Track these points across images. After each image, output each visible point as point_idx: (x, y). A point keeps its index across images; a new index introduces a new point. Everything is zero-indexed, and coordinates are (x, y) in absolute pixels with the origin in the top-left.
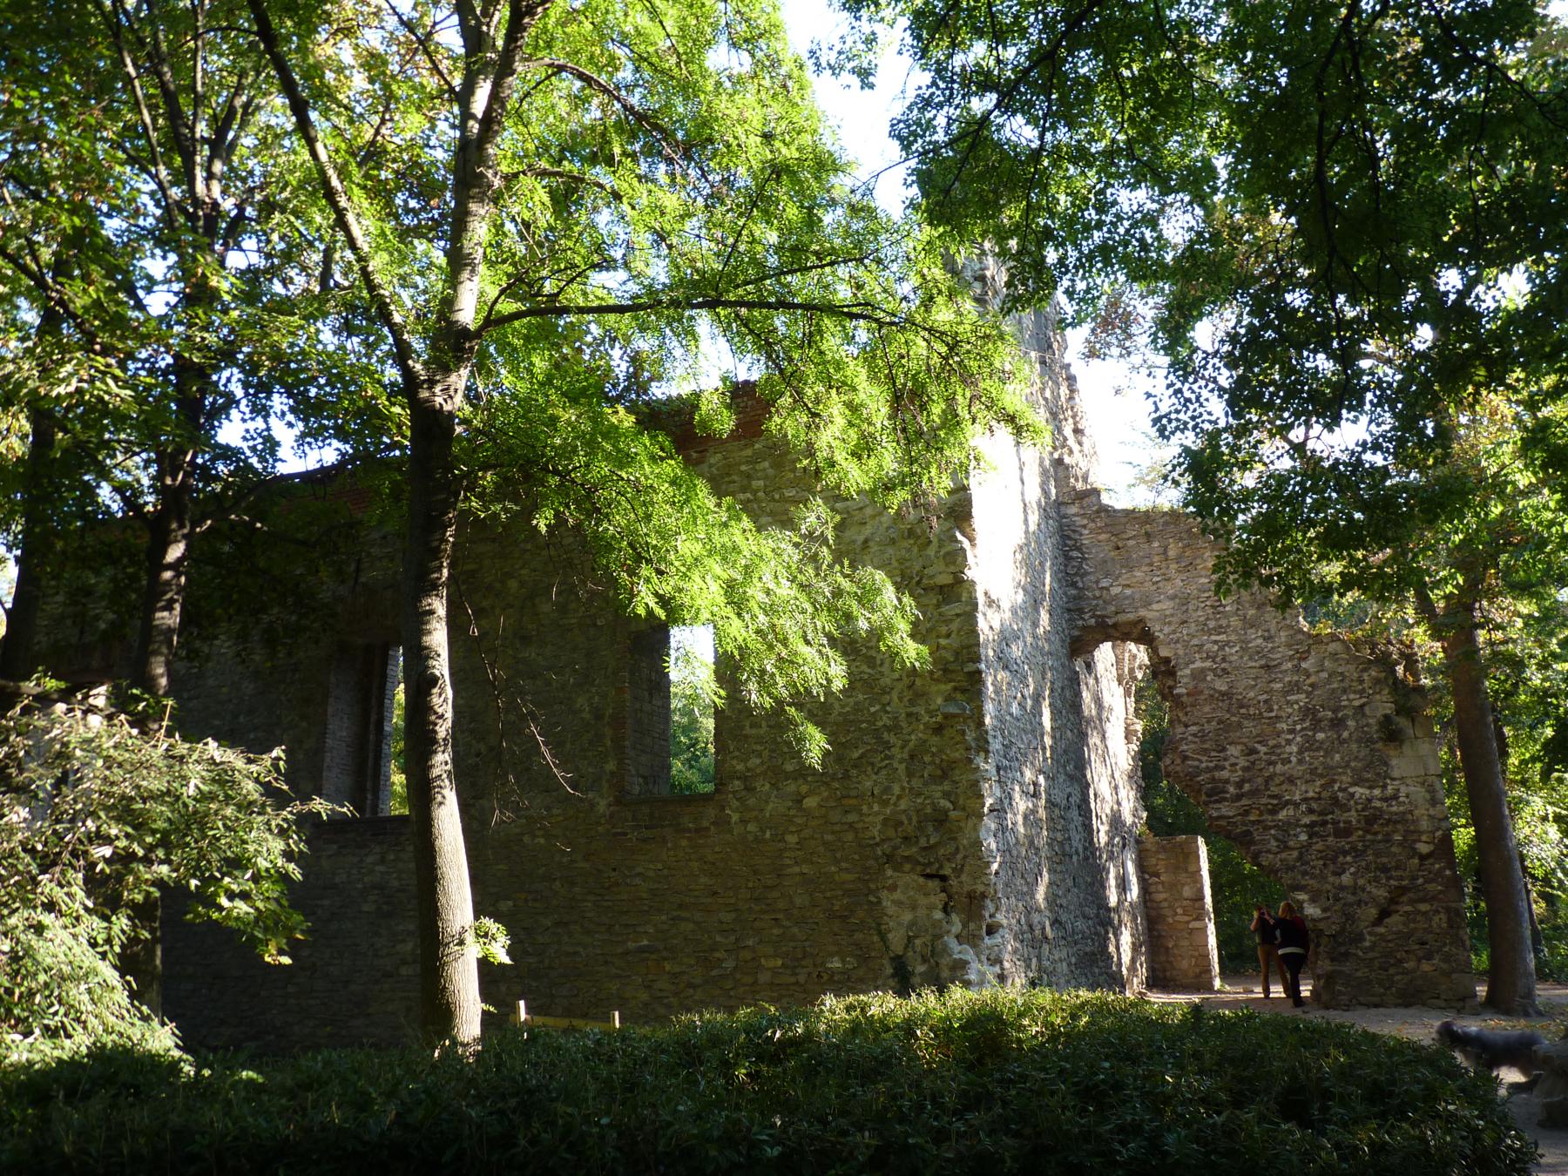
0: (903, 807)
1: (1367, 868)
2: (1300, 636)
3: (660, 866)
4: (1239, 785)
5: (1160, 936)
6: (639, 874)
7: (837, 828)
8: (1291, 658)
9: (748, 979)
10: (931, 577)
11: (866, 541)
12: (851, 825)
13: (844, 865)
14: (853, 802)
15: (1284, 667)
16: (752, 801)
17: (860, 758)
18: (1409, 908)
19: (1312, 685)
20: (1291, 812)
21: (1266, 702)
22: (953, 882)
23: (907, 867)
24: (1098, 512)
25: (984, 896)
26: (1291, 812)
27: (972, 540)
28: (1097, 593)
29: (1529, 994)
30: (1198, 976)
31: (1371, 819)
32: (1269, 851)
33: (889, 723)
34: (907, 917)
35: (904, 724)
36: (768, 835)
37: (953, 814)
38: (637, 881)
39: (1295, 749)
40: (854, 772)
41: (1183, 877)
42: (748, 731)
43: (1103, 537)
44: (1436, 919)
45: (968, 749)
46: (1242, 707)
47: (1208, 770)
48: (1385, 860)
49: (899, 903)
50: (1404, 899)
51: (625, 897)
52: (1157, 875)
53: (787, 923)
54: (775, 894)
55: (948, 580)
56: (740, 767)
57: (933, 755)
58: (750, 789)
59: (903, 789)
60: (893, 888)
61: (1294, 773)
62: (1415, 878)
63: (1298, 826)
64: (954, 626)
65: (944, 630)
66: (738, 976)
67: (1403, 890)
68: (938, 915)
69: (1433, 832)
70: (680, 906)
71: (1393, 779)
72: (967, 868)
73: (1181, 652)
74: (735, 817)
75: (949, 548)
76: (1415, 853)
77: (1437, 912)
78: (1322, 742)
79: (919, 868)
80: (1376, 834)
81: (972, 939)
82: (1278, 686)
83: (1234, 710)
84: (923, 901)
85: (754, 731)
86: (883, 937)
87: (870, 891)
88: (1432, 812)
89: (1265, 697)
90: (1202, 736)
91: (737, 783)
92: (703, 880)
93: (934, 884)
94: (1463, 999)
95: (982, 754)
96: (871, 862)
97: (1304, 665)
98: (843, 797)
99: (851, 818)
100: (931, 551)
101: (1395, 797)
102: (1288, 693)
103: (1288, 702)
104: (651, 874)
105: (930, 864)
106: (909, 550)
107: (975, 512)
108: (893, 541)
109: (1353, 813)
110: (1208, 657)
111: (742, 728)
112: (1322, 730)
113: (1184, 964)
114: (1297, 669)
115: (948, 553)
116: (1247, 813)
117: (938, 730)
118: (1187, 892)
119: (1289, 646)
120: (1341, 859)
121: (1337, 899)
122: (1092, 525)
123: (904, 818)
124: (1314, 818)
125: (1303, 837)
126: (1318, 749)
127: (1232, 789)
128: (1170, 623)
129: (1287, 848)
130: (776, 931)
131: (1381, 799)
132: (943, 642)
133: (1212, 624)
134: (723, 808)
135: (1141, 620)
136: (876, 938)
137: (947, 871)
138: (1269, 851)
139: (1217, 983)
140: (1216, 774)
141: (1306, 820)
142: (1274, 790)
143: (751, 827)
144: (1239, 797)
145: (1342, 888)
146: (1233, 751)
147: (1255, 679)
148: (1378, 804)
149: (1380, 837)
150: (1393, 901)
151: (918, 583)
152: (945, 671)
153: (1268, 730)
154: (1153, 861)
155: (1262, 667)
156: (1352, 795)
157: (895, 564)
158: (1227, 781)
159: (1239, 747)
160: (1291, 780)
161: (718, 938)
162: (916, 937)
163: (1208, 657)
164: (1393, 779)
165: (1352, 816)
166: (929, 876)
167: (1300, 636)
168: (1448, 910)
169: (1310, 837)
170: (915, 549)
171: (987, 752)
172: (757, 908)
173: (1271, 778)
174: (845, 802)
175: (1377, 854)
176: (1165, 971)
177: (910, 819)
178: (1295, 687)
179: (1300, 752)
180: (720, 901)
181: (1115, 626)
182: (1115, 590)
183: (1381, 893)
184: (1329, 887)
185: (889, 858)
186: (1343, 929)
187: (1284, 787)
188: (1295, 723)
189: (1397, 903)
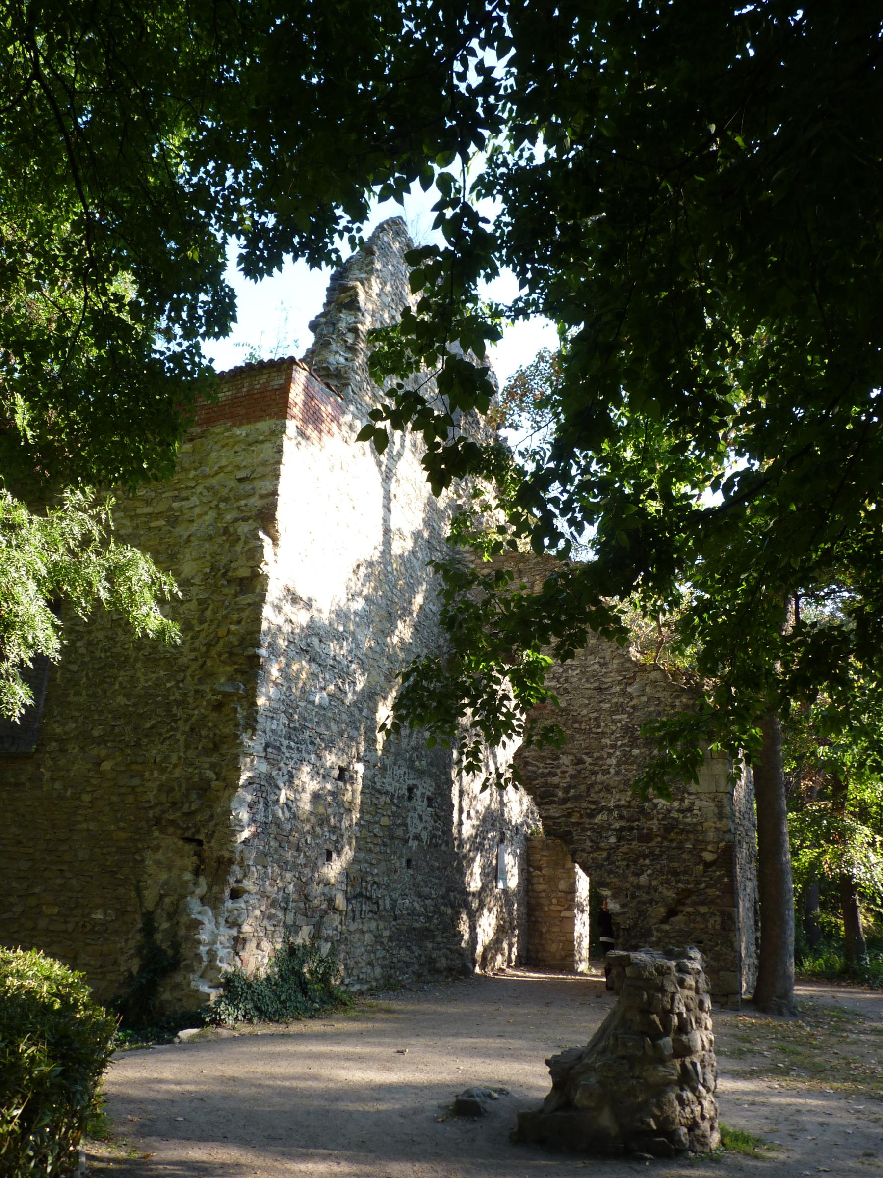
0: (176, 775)
1: (661, 872)
2: (628, 665)
4: (566, 790)
5: (536, 922)
7: (123, 790)
8: (620, 682)
10: (235, 570)
11: (190, 536)
12: (133, 788)
13: (122, 824)
14: (139, 767)
15: (613, 690)
17: (152, 727)
18: (690, 909)
19: (633, 707)
20: (605, 817)
21: (596, 719)
22: (205, 847)
23: (171, 830)
25: (231, 862)
26: (605, 817)
27: (275, 540)
29: (786, 993)
30: (563, 958)
31: (670, 827)
32: (583, 850)
33: (179, 698)
34: (164, 876)
35: (191, 701)
36: (69, 793)
37: (214, 784)
39: (614, 761)
41: (560, 872)
42: (72, 699)
44: (712, 921)
45: (237, 725)
46: (575, 722)
47: (544, 775)
48: (676, 865)
49: (158, 863)
50: (688, 901)
52: (540, 869)
55: (244, 573)
57: (210, 729)
58: (63, 751)
59: (179, 758)
60: (157, 848)
61: (611, 783)
62: (698, 883)
63: (609, 829)
64: (244, 615)
65: (235, 617)
67: (688, 893)
68: (188, 876)
69: (718, 843)
71: (690, 794)
72: (217, 835)
74: (47, 775)
75: (251, 545)
76: (701, 860)
77: (713, 914)
78: (636, 757)
79: (179, 832)
80: (671, 841)
81: (212, 901)
82: (606, 706)
83: (569, 724)
84: (178, 862)
86: (139, 890)
88: (718, 825)
89: (595, 714)
91: (54, 744)
93: (189, 848)
94: (726, 995)
95: (250, 732)
96: (143, 824)
97: (629, 689)
98: (132, 763)
99: (136, 782)
100: (239, 548)
101: (690, 810)
102: (613, 713)
103: (613, 721)
105: (188, 828)
106: (221, 546)
107: (278, 515)
108: (210, 538)
109: (655, 821)
110: (554, 678)
112: (638, 747)
113: (553, 948)
114: (623, 692)
115: (250, 550)
116: (569, 815)
117: (218, 707)
118: (562, 885)
119: (619, 672)
120: (641, 861)
121: (634, 897)
123: (175, 785)
124: (623, 823)
125: (613, 840)
126: (632, 764)
127: (560, 794)
129: (598, 848)
130: (59, 881)
131: (679, 811)
132: (233, 628)
134: (38, 766)
136: (133, 894)
137: (201, 837)
138: (583, 850)
139: (583, 967)
140: (550, 780)
141: (617, 825)
142: (594, 797)
143: (58, 785)
144: (564, 801)
145: (639, 887)
146: (565, 760)
147: (589, 698)
148: (675, 814)
149: (674, 844)
150: (680, 902)
151: (224, 575)
152: (231, 654)
153: (594, 744)
154: (538, 857)
155: (595, 689)
156: (656, 805)
157: (208, 557)
158: (557, 786)
159: (570, 757)
160: (608, 789)
161: (15, 885)
162: (166, 895)
163: (554, 678)
164: (690, 794)
165: (654, 824)
166: (188, 840)
167: (628, 665)
168: (723, 913)
169: (619, 840)
170: (227, 545)
171: (254, 730)
173: (592, 785)
174: (134, 767)
175: (671, 859)
176: (537, 952)
177: (180, 786)
178: (619, 708)
179: (618, 765)
183: (670, 894)
184: (628, 885)
185: (158, 821)
186: (636, 924)
187: (602, 795)
188: (617, 739)
189: (684, 904)
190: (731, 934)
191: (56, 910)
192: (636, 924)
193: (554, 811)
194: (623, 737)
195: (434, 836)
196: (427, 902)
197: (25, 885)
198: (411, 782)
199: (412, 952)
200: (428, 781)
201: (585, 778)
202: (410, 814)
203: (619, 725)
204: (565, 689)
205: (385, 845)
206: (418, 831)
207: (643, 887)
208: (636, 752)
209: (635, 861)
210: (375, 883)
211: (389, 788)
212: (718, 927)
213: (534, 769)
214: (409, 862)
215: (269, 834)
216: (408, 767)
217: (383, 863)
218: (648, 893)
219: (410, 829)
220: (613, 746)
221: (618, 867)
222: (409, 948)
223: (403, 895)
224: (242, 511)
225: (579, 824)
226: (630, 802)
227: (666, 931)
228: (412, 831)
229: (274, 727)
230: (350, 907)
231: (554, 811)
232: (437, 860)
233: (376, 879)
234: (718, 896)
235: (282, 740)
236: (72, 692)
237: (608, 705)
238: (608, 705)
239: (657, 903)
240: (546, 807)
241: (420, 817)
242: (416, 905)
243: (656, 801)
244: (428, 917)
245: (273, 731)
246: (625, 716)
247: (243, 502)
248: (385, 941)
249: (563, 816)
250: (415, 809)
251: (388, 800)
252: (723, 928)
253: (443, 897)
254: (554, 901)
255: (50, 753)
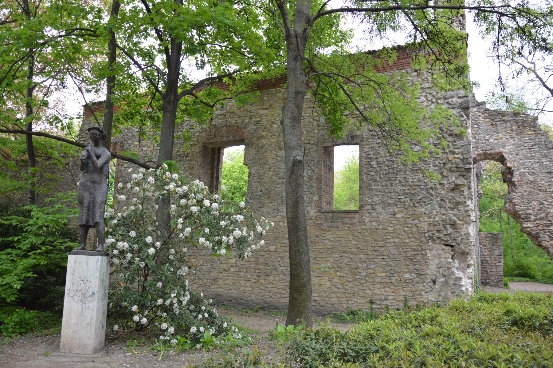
3: (336, 236)
6: (327, 239)
7: (410, 226)
9: (372, 280)
12: (415, 225)
13: (412, 239)
16: (374, 214)
21: (549, 185)
23: (438, 241)
24: (485, 110)
28: (484, 141)
32: (545, 241)
38: (326, 241)
40: (417, 205)
43: (487, 120)
51: (321, 247)
53: (388, 260)
54: (383, 249)
56: (370, 201)
59: (437, 212)
66: (367, 279)
68: (450, 260)
70: (344, 252)
73: (516, 165)
74: (367, 220)
79: (443, 242)
85: (375, 187)
87: (423, 250)
89: (548, 183)
90: (522, 197)
91: (368, 206)
92: (353, 242)
96: (423, 239)
99: (416, 222)
104: (332, 239)
111: (371, 186)
122: (483, 116)
128: (512, 154)
130: (383, 263)
133: (529, 155)
135: (501, 153)
140: (527, 211)
143: (374, 224)
144: (535, 220)
158: (531, 214)
159: (537, 202)
161: (359, 265)
172: (376, 254)
180: (360, 250)
181: (490, 154)
182: (491, 141)
191: (384, 274)
197: (365, 265)
204: (532, 172)
224: (450, 104)
236: (373, 184)
247: (450, 100)
255: (367, 210)
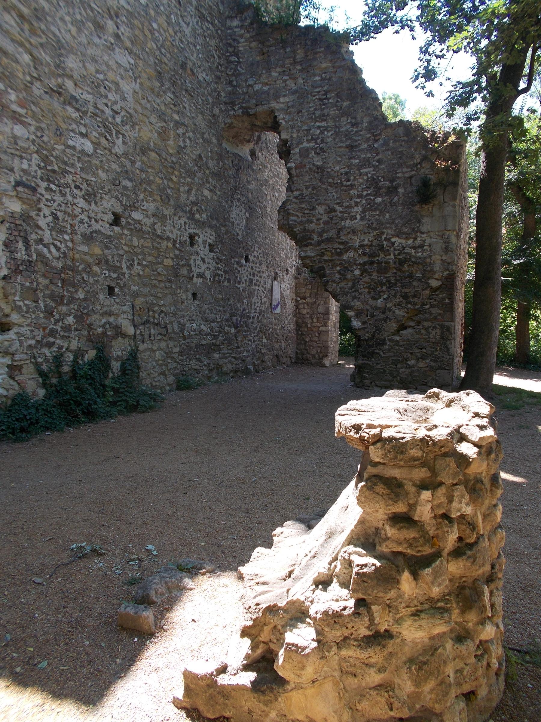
4: (320, 235)
19: (379, 161)
21: (346, 173)
32: (334, 281)
48: (407, 290)
62: (424, 304)
71: (422, 233)
76: (429, 286)
77: (435, 328)
78: (379, 205)
89: (346, 170)
101: (421, 246)
110: (313, 139)
112: (381, 196)
114: (371, 148)
116: (323, 254)
118: (321, 309)
121: (373, 316)
124: (366, 259)
125: (357, 272)
126: (375, 210)
138: (334, 281)
142: (344, 238)
144: (319, 243)
145: (377, 308)
146: (320, 209)
148: (408, 250)
155: (347, 147)
156: (393, 244)
158: (313, 231)
159: (324, 207)
160: (354, 232)
163: (313, 139)
168: (442, 327)
178: (366, 163)
179: (363, 212)
186: (373, 336)
187: (350, 236)
190: (448, 343)
192: (373, 336)
193: (310, 252)
194: (369, 188)
195: (217, 275)
196: (212, 324)
198: (192, 231)
199: (201, 362)
200: (209, 231)
201: (336, 224)
202: (193, 257)
203: (365, 178)
204: (321, 149)
205: (170, 281)
206: (202, 271)
207: (380, 308)
208: (379, 200)
209: (374, 289)
210: (162, 312)
211: (170, 235)
212: (438, 337)
213: (295, 218)
214: (194, 295)
215: (37, 272)
216: (188, 218)
217: (170, 296)
218: (384, 313)
219: (193, 268)
220: (359, 196)
221: (360, 294)
222: (199, 360)
223: (192, 320)
225: (331, 261)
226: (372, 241)
227: (397, 341)
228: (196, 271)
229: (25, 166)
230: (138, 332)
231: (310, 252)
232: (220, 292)
233: (163, 309)
234: (440, 314)
235: (39, 181)
237: (357, 161)
238: (357, 161)
239: (390, 320)
240: (305, 249)
241: (203, 260)
242: (203, 327)
243: (393, 240)
244: (214, 336)
245: (23, 170)
246: (372, 169)
248: (176, 356)
249: (318, 255)
250: (197, 253)
251: (170, 245)
252: (442, 338)
253: (227, 320)
254: (315, 320)
